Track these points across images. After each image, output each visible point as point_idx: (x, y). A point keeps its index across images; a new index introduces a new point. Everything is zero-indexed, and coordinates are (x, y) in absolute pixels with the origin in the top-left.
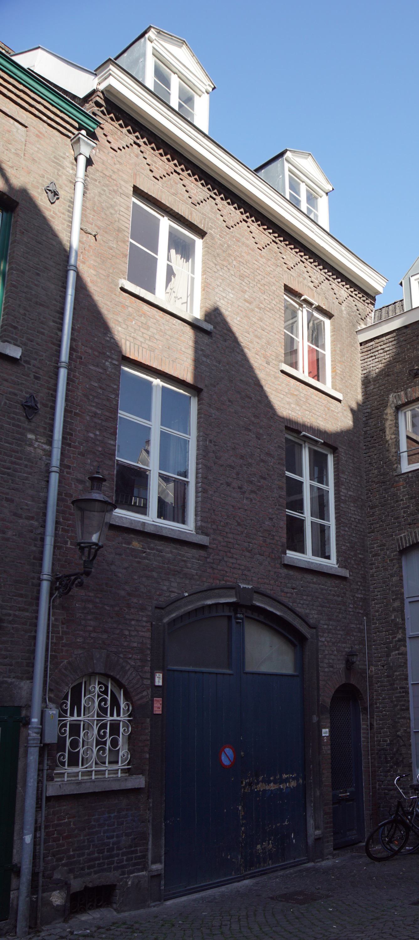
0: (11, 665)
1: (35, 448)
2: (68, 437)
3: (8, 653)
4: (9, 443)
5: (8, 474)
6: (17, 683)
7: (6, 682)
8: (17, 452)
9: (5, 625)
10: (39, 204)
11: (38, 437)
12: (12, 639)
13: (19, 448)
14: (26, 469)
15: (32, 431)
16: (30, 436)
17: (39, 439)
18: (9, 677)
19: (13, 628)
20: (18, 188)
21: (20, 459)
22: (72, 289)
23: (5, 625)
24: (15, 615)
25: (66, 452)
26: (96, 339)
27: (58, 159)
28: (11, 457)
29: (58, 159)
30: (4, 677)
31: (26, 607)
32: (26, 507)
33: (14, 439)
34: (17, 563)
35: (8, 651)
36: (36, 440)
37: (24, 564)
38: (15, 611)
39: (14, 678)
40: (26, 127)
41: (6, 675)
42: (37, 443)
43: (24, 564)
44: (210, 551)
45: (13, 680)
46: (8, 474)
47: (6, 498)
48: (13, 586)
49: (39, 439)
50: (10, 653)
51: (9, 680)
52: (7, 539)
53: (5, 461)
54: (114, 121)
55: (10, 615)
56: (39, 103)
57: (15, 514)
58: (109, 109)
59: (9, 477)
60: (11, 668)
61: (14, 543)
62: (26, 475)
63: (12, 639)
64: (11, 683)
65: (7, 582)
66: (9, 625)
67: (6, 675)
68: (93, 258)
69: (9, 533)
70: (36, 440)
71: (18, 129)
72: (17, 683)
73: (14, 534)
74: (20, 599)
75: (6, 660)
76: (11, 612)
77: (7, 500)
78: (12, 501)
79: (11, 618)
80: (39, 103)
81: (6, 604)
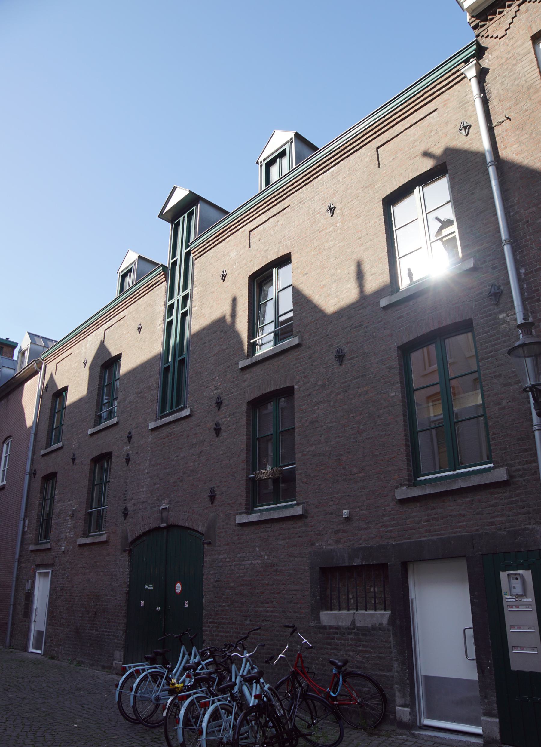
0: (529, 513)
1: (509, 322)
2: (535, 294)
3: (524, 503)
4: (486, 333)
5: (492, 357)
6: (538, 528)
7: (527, 529)
8: (495, 335)
9: (517, 479)
10: (458, 147)
11: (508, 312)
12: (525, 490)
13: (494, 332)
14: (505, 344)
15: (502, 312)
16: (501, 316)
17: (509, 313)
18: (530, 524)
19: (524, 480)
20: (437, 155)
21: (498, 339)
22: (494, 179)
23: (517, 479)
24: (524, 469)
25: (537, 308)
26: (536, 195)
27: (462, 102)
28: (491, 341)
29: (462, 102)
30: (525, 525)
31: (532, 459)
32: (513, 375)
33: (489, 327)
34: (516, 424)
35: (524, 501)
36: (508, 316)
37: (523, 422)
38: (524, 465)
39: (534, 524)
40: (436, 109)
41: (526, 523)
42: (509, 318)
43: (523, 422)
44: (537, 324)
45: (534, 526)
46: (492, 357)
47: (495, 376)
48: (517, 445)
49: (509, 313)
50: (526, 502)
51: (530, 527)
52: (504, 408)
53: (487, 348)
54: (494, 18)
55: (519, 470)
56: (435, 86)
57: (506, 385)
58: (483, 18)
59: (493, 359)
60: (530, 515)
61: (510, 409)
62: (506, 349)
63: (525, 490)
64: (533, 529)
65: (511, 443)
66: (521, 479)
67: (526, 523)
68: (513, 135)
69: (504, 403)
70: (508, 316)
71: (433, 117)
72: (538, 528)
73: (508, 401)
74: (526, 453)
75: (524, 510)
76: (519, 467)
77: (496, 377)
78: (500, 376)
79: (521, 472)
80: (435, 86)
81: (514, 461)
